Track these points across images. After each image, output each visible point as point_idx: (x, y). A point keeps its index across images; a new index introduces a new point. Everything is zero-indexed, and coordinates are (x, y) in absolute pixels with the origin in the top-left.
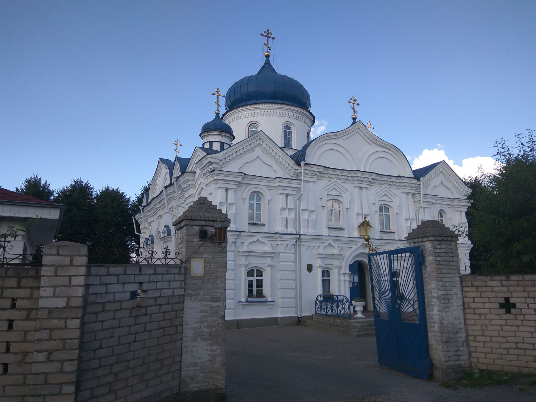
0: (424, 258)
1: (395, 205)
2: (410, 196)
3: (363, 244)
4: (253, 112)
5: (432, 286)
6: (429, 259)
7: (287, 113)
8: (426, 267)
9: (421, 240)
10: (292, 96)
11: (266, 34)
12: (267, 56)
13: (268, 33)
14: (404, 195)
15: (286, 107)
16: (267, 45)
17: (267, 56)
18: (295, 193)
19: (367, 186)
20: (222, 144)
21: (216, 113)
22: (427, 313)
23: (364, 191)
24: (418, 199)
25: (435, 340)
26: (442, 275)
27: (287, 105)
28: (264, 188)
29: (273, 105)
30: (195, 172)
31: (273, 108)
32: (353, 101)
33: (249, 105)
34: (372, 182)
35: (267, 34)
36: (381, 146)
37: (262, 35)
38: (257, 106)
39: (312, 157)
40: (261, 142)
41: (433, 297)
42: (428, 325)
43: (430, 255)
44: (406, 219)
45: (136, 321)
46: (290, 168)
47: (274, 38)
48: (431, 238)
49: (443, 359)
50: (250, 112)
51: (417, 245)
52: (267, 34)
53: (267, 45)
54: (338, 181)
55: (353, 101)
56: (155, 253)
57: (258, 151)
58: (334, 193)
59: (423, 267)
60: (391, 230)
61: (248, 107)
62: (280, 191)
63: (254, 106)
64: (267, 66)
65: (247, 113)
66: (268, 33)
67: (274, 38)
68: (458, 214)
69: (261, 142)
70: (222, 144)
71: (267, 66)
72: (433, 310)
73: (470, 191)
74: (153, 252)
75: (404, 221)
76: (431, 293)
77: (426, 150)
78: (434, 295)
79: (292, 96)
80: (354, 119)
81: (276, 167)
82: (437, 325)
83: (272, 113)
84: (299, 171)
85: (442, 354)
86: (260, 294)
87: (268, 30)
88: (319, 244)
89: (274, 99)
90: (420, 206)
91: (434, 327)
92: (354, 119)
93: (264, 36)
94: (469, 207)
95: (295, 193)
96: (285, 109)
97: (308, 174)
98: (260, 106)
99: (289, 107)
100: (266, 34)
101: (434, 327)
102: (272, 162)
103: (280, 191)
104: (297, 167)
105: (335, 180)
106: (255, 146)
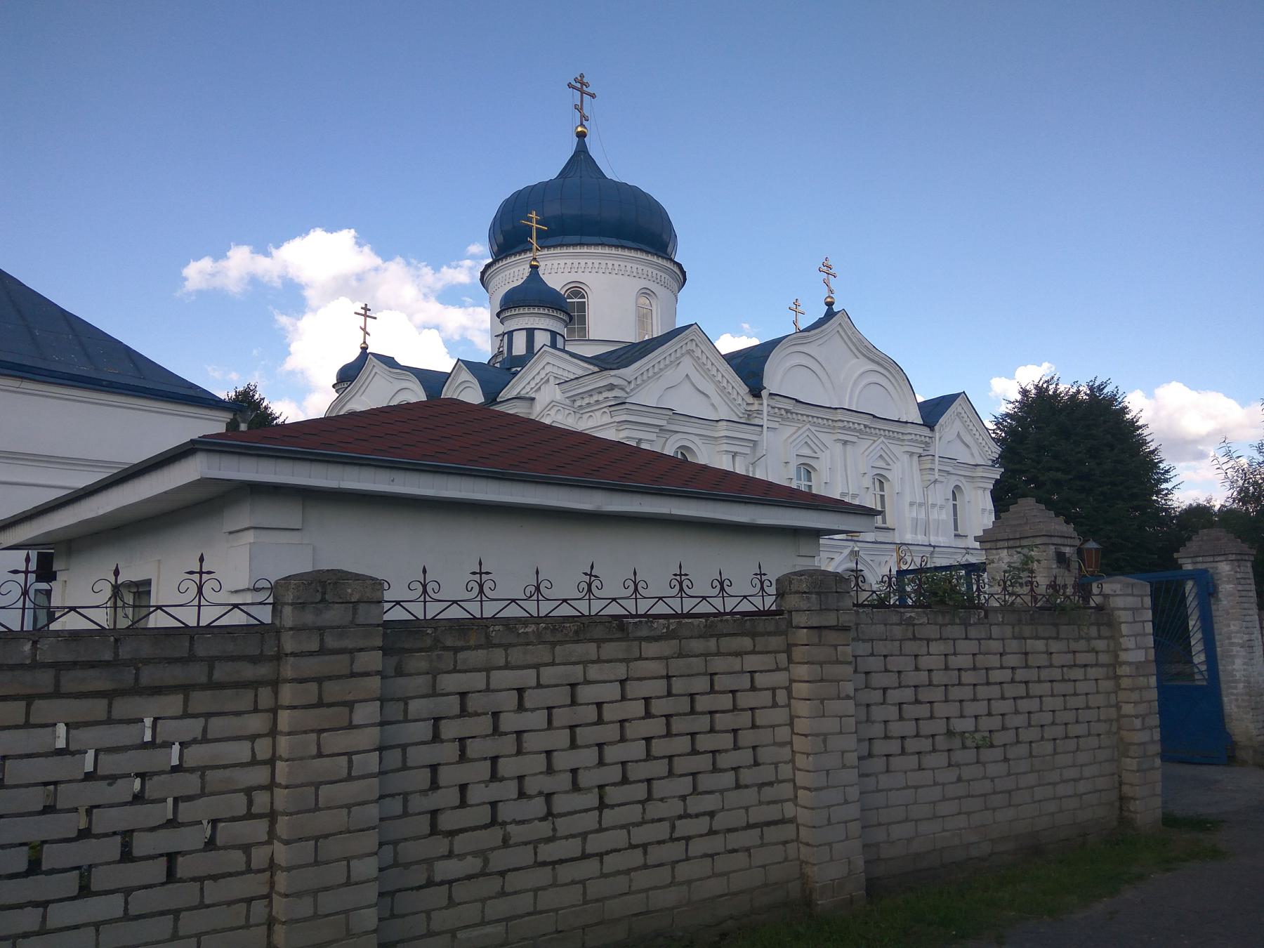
0: (1215, 587)
1: (894, 475)
2: (915, 458)
3: (852, 552)
4: (575, 262)
5: (1232, 628)
6: (1226, 588)
7: (646, 269)
8: (1218, 600)
9: (1211, 559)
10: (638, 228)
11: (579, 85)
12: (581, 136)
13: (582, 84)
14: (906, 457)
15: (644, 256)
16: (579, 108)
17: (581, 136)
18: (747, 451)
19: (854, 439)
20: (554, 334)
21: (532, 266)
22: (1221, 668)
23: (849, 447)
24: (929, 466)
25: (1238, 707)
26: (1245, 612)
27: (647, 252)
28: (696, 439)
29: (620, 252)
30: (533, 399)
31: (617, 257)
32: (827, 269)
33: (568, 245)
34: (864, 432)
35: (580, 85)
36: (878, 363)
37: (570, 85)
38: (585, 250)
39: (776, 377)
40: (693, 346)
41: (1232, 644)
42: (1223, 686)
43: (1229, 582)
44: (911, 504)
45: (753, 716)
46: (740, 401)
47: (593, 96)
48: (1234, 557)
49: (1255, 732)
50: (569, 262)
51: (1200, 566)
52: (580, 85)
53: (579, 108)
54: (813, 429)
55: (827, 269)
56: (727, 582)
57: (687, 365)
58: (807, 452)
59: (1212, 601)
60: (888, 525)
61: (564, 250)
62: (725, 447)
63: (578, 250)
64: (581, 159)
65: (562, 262)
66: (582, 84)
67: (593, 96)
68: (980, 492)
69: (693, 346)
70: (554, 334)
71: (581, 159)
72: (1233, 663)
73: (998, 450)
74: (722, 583)
75: (907, 507)
76: (1230, 638)
77: (728, 335)
78: (1234, 640)
79: (638, 228)
80: (830, 304)
81: (716, 399)
82: (1241, 686)
83: (596, 265)
84: (756, 407)
85: (1251, 726)
86: (130, 852)
87: (582, 76)
88: (887, 558)
89: (618, 237)
90: (932, 478)
91: (1235, 688)
92: (830, 304)
93: (574, 88)
94: (997, 481)
95: (747, 451)
96: (651, 264)
97: (774, 415)
98: (592, 250)
99: (650, 258)
100: (579, 85)
101: (1235, 688)
102: (710, 388)
103: (725, 447)
104: (750, 399)
105: (808, 426)
106: (683, 355)
